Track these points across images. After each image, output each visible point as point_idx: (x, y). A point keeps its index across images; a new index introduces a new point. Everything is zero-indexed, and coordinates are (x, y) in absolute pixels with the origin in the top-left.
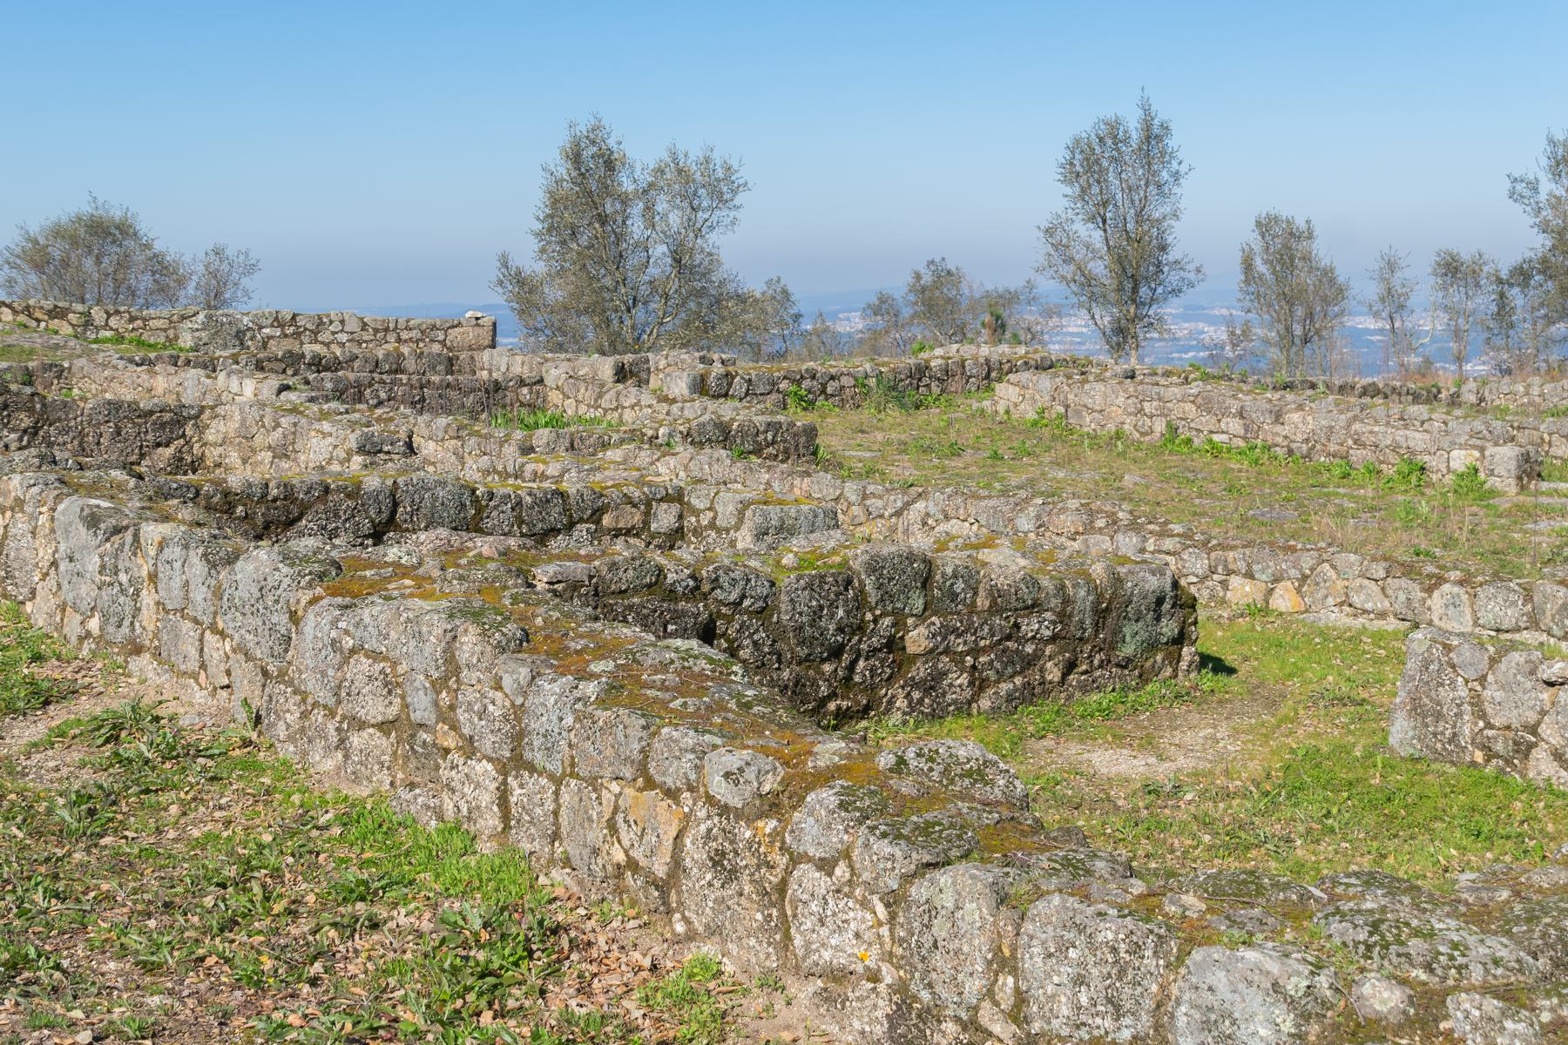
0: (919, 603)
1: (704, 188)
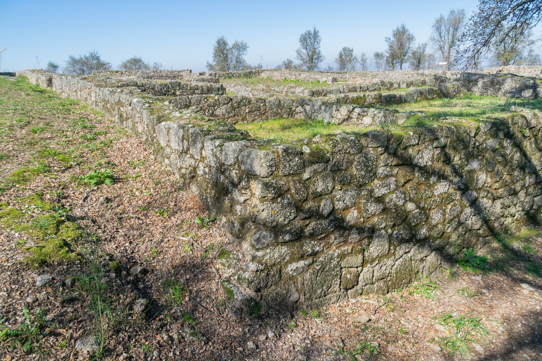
0: (178, 88)
1: (241, 47)
